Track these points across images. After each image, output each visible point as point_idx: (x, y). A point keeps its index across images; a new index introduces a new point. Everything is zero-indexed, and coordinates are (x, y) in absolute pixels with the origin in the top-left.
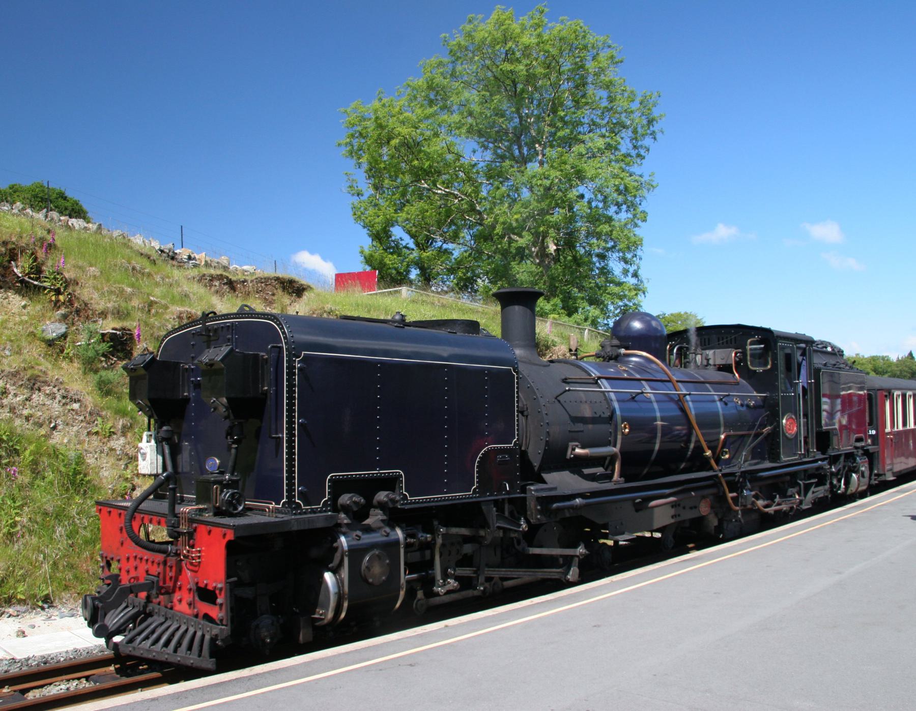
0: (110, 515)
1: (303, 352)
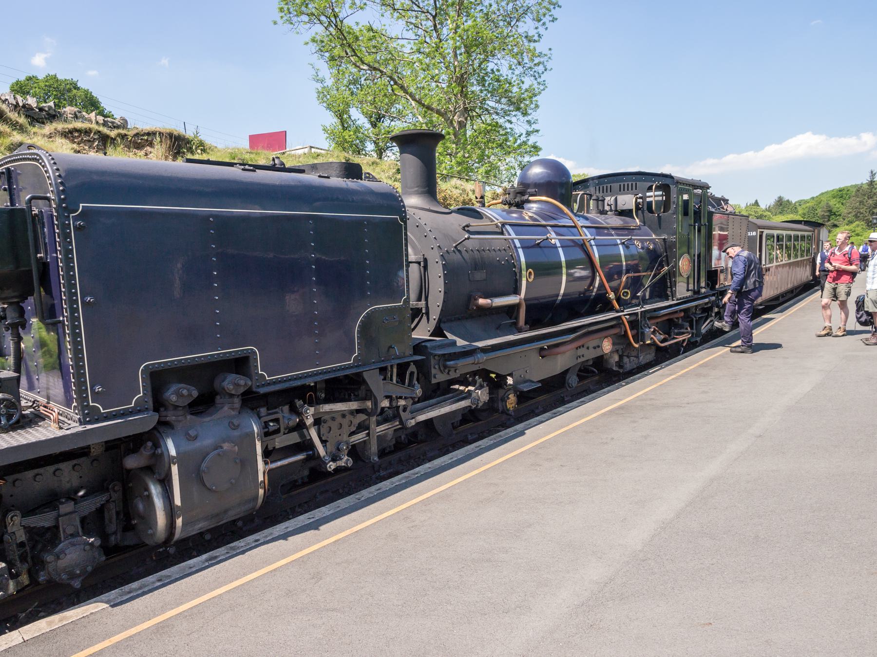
1: (81, 205)
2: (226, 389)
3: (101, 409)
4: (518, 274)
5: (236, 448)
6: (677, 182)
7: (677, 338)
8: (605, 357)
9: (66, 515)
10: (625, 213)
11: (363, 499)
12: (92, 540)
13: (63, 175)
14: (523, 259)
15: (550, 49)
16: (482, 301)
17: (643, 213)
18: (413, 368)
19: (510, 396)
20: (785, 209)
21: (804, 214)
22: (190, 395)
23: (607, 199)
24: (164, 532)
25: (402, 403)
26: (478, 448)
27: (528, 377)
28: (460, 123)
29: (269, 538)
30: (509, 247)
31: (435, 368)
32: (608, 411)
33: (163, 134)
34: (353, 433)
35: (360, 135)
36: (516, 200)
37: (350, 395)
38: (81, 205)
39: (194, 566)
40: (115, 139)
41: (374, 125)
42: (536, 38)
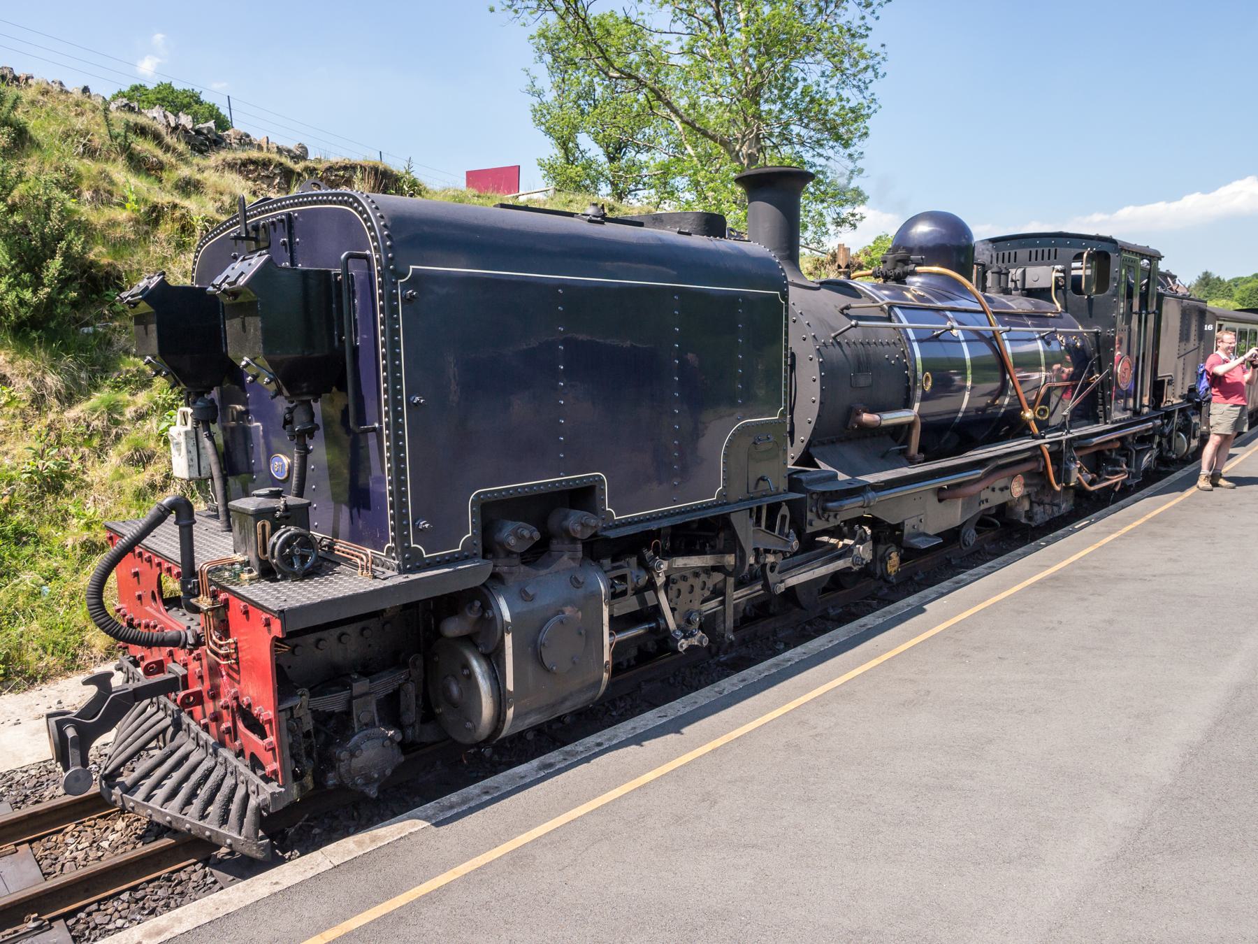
0: (248, 619)
1: (411, 267)
2: (571, 531)
3: (424, 553)
4: (911, 380)
5: (580, 613)
6: (1122, 249)
7: (1108, 480)
8: (1009, 504)
9: (361, 696)
10: (1041, 293)
11: (726, 693)
12: (392, 732)
13: (389, 225)
14: (918, 355)
15: (883, 45)
16: (866, 417)
17: (1065, 292)
18: (785, 510)
19: (892, 555)
20: (1214, 291)
21: (1243, 299)
22: (531, 538)
23: (1013, 271)
24: (488, 726)
25: (770, 559)
26: (864, 629)
27: (921, 529)
28: (750, 156)
29: (615, 742)
30: (899, 340)
31: (811, 511)
32: (1036, 582)
33: (365, 170)
34: (703, 602)
35: (593, 173)
36: (897, 271)
37: (703, 546)
38: (411, 267)
39: (525, 776)
40: (299, 175)
41: (612, 159)
42: (862, 31)
